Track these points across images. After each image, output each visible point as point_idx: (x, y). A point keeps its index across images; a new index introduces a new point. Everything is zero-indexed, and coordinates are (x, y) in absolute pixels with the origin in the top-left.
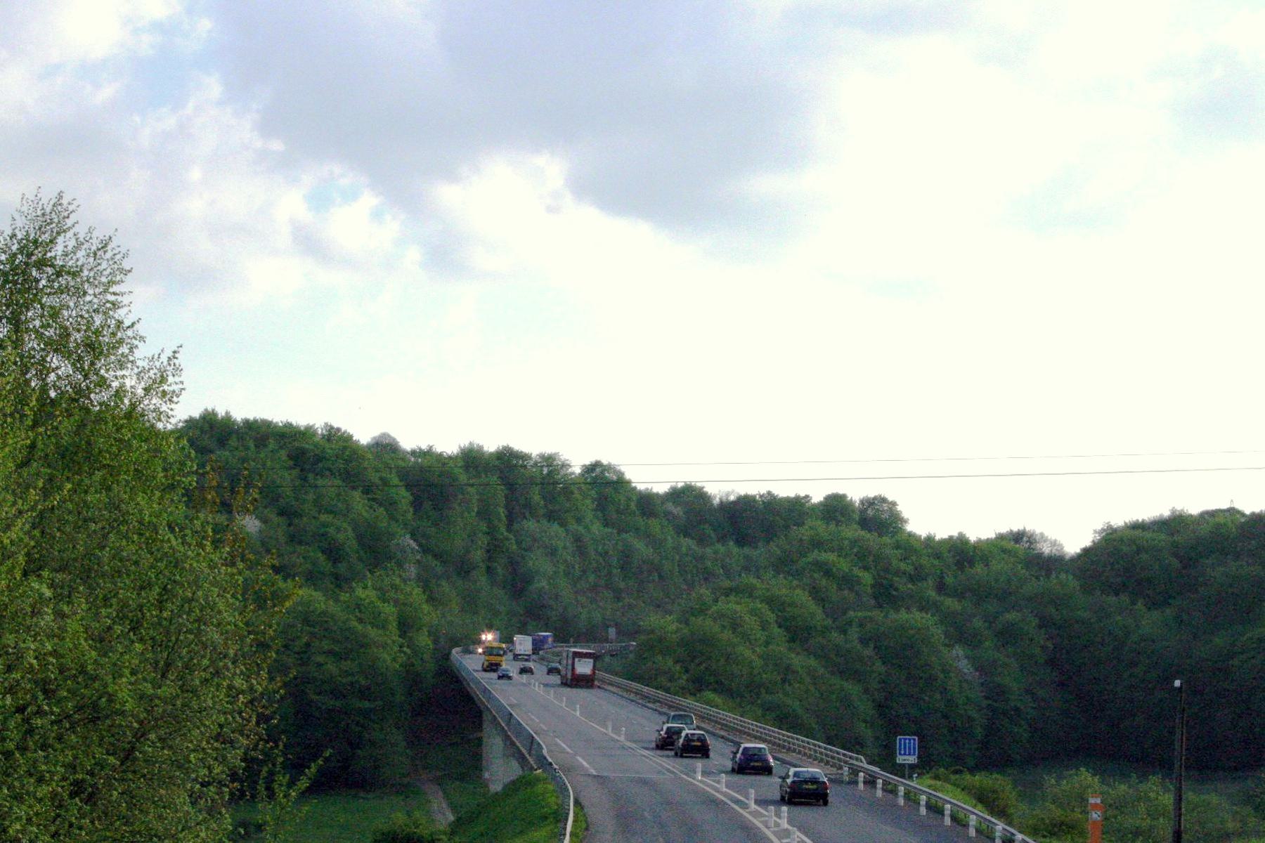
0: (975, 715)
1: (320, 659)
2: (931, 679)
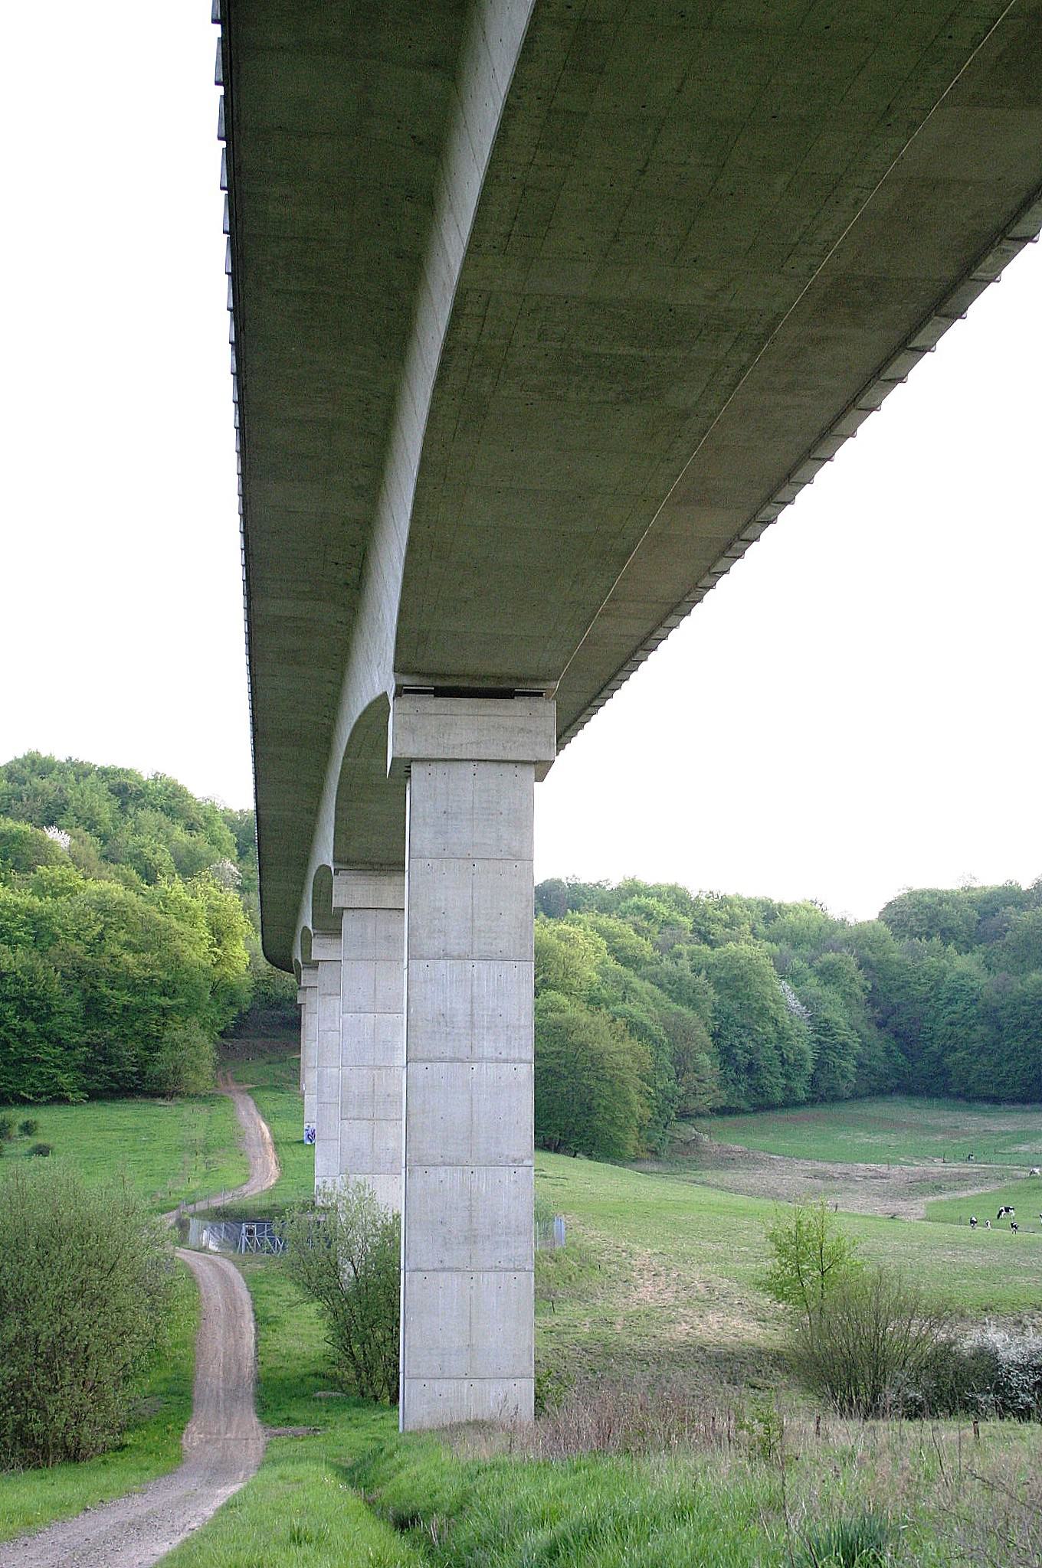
0: (805, 1047)
1: (116, 949)
2: (763, 1011)
